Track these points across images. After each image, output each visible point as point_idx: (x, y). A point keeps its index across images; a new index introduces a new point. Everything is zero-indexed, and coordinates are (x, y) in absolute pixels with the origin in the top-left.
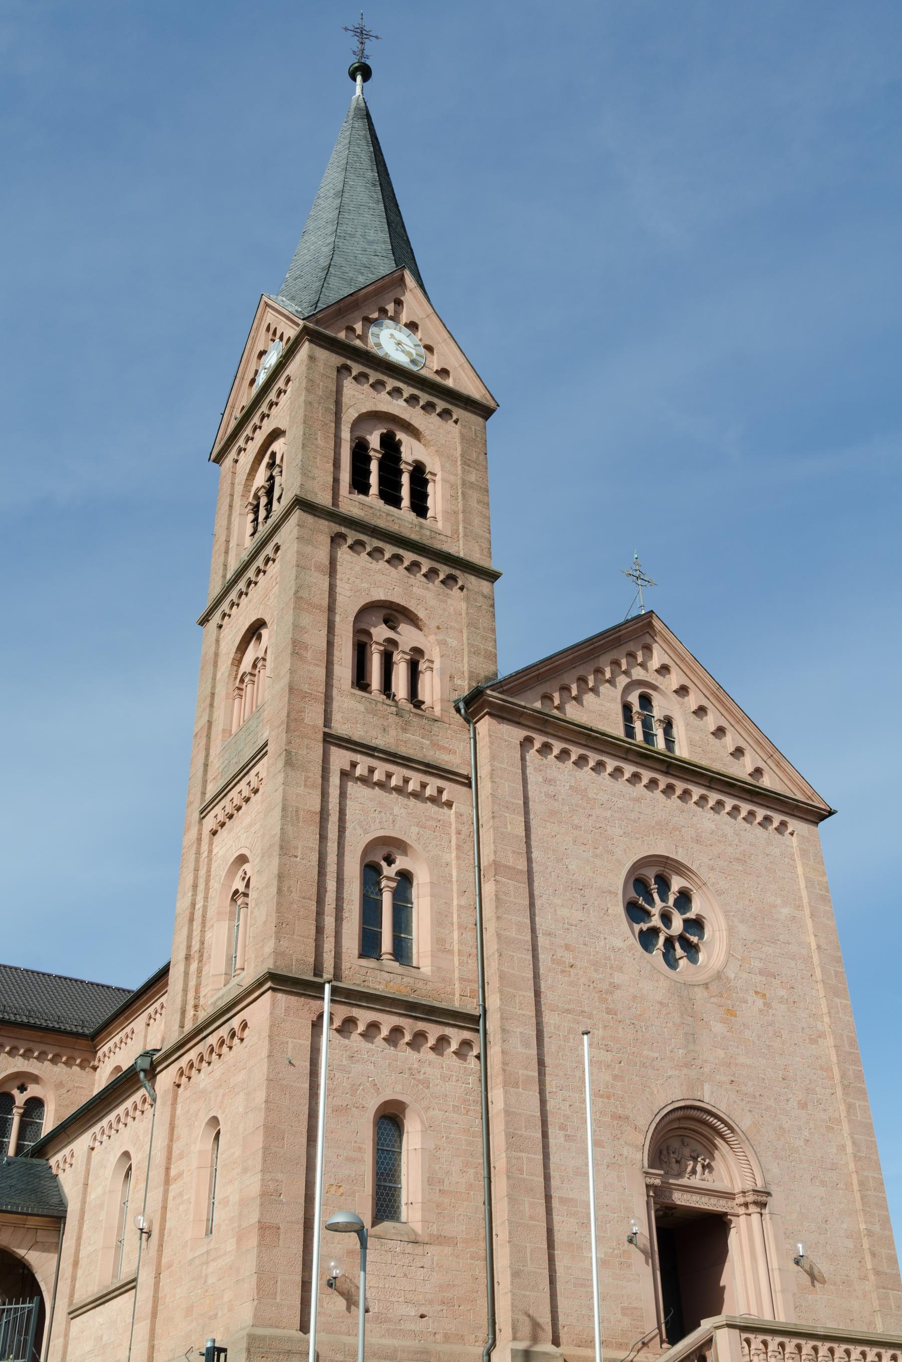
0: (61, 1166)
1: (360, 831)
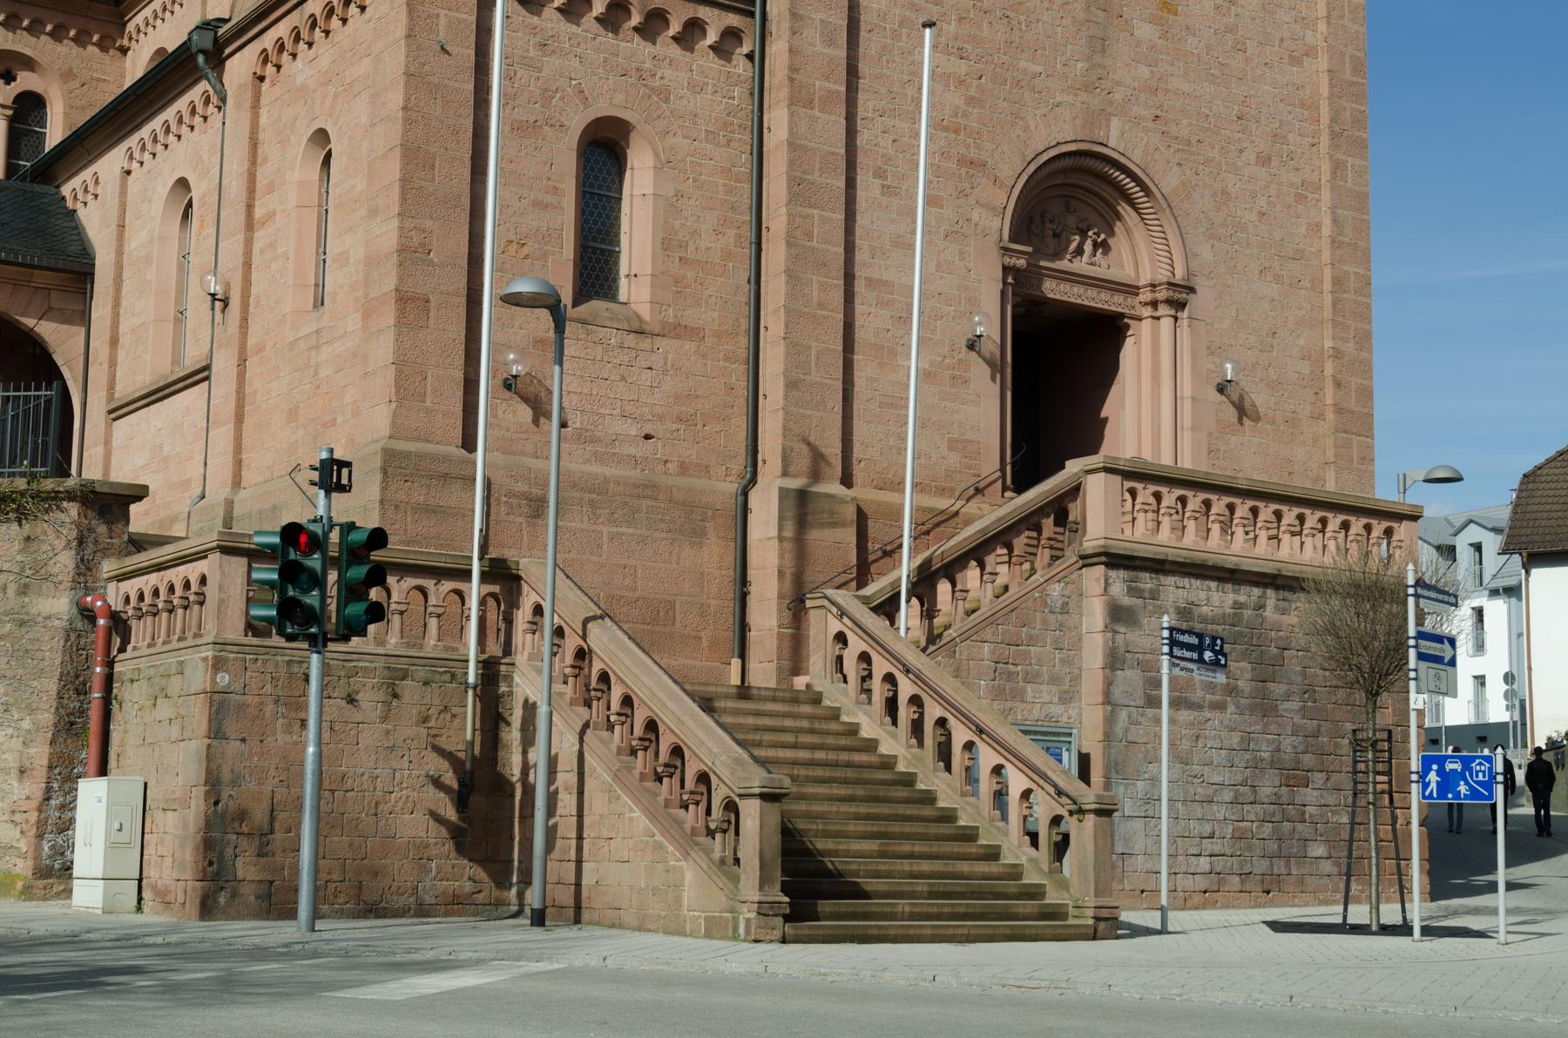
0: (80, 196)
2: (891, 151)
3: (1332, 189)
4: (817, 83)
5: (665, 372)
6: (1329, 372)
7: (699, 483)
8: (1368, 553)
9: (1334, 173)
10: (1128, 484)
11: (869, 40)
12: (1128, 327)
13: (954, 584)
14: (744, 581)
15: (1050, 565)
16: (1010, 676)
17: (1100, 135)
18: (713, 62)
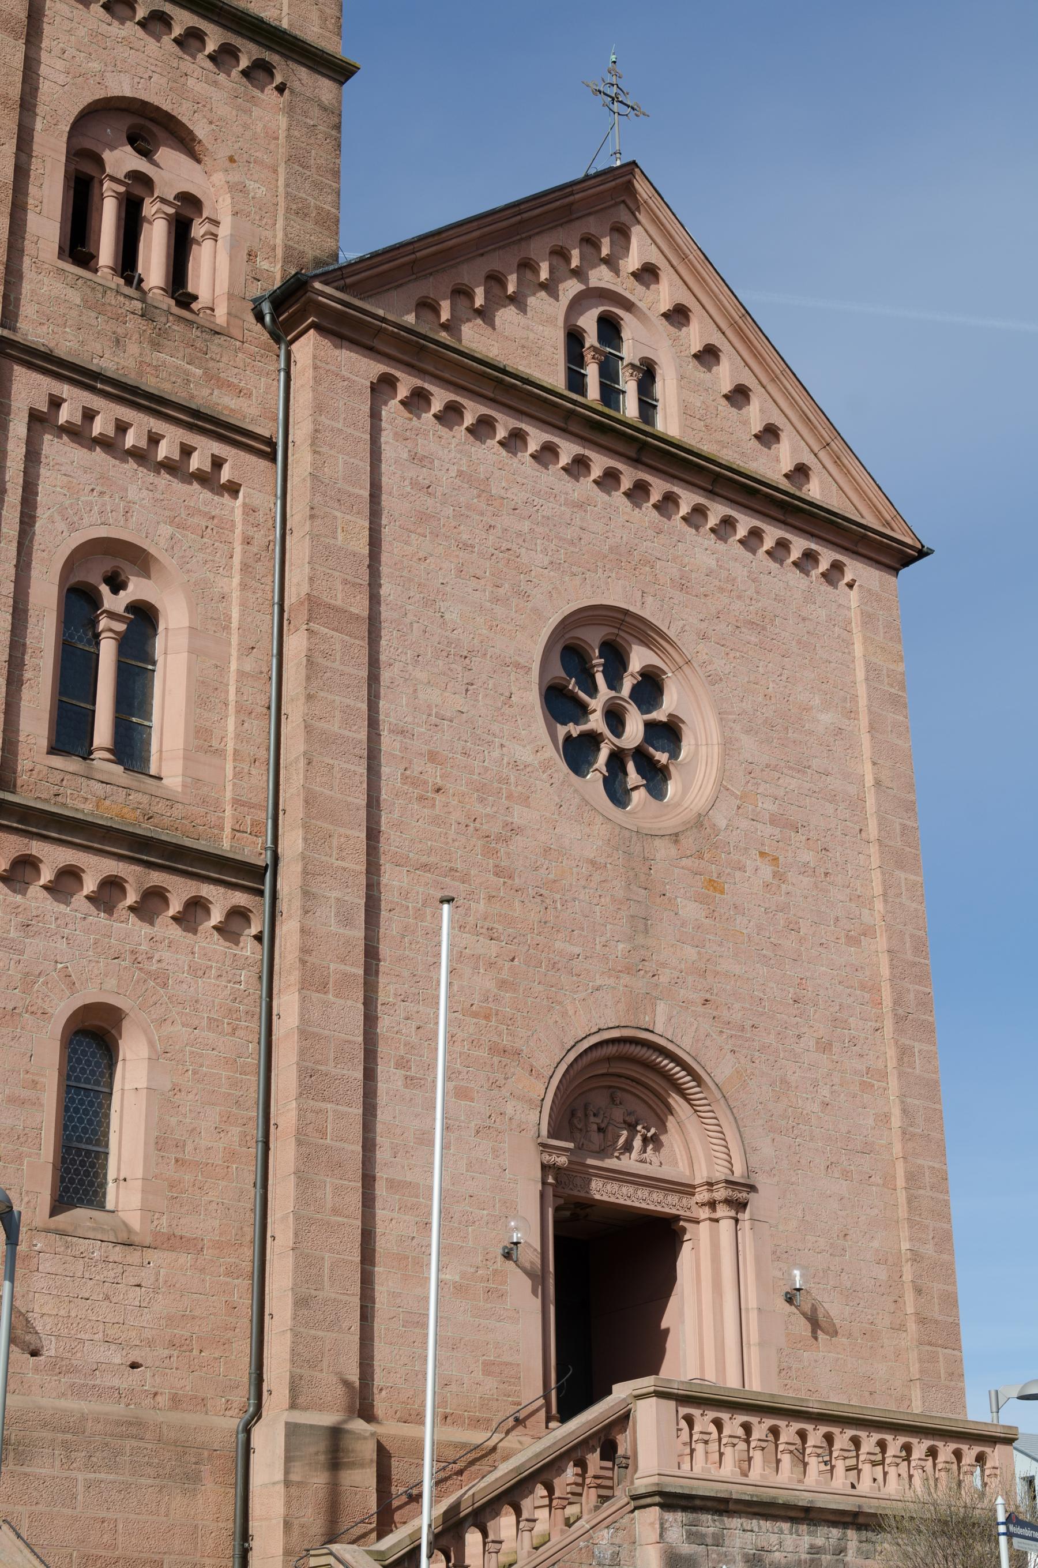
1: (61, 526)
2: (414, 1039)
3: (900, 1075)
4: (332, 966)
5: (156, 1290)
6: (908, 1277)
7: (193, 1418)
8: (959, 1483)
9: (900, 1060)
10: (684, 1411)
11: (390, 919)
12: (684, 1230)
13: (485, 1534)
14: (245, 1535)
15: (597, 1508)
17: (646, 1021)
18: (218, 944)
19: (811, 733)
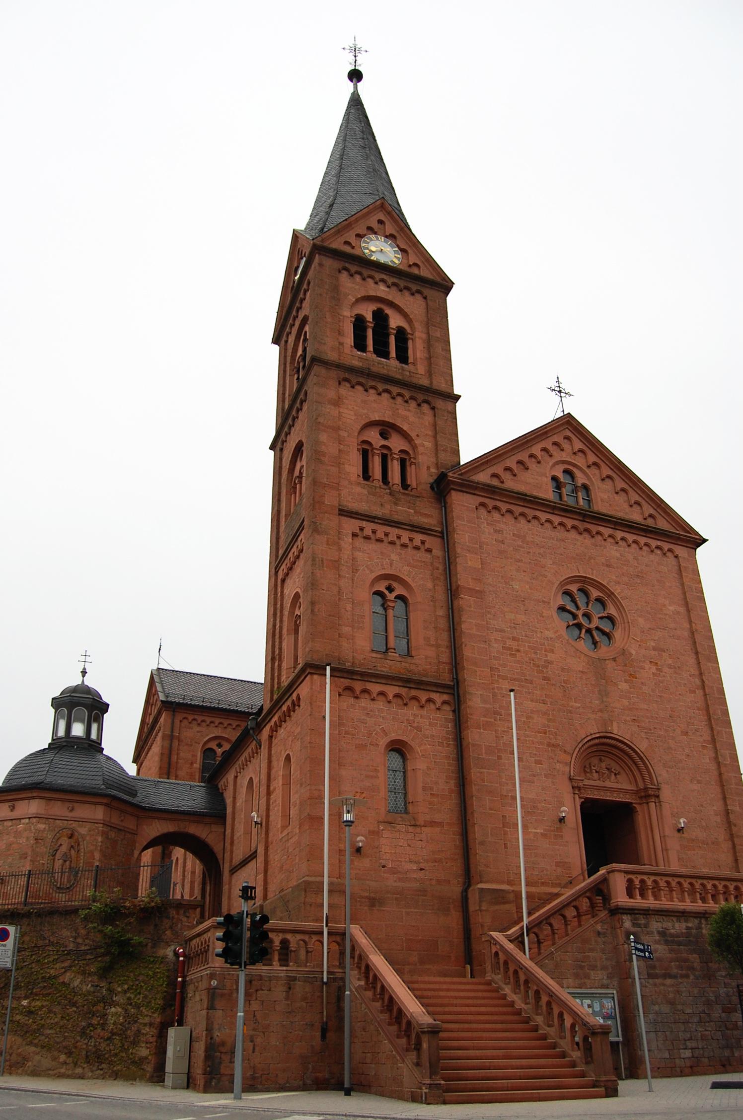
1: (368, 572)
16: (582, 967)
19: (666, 614)
